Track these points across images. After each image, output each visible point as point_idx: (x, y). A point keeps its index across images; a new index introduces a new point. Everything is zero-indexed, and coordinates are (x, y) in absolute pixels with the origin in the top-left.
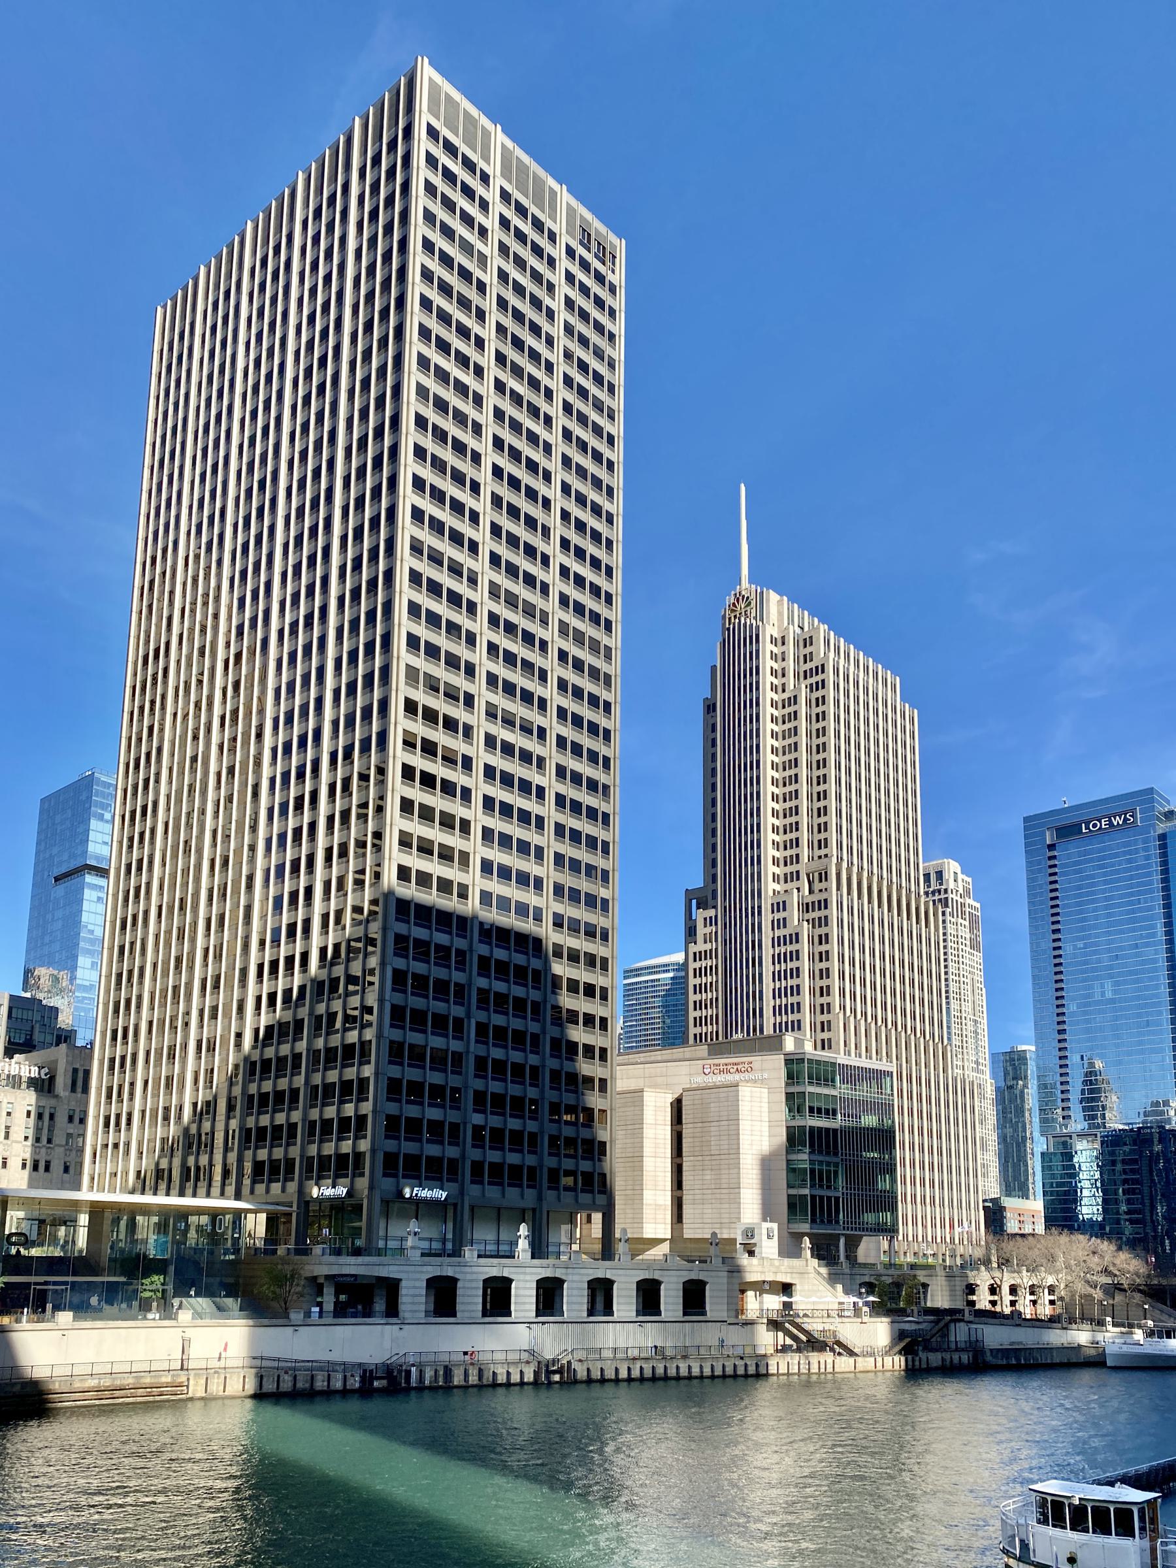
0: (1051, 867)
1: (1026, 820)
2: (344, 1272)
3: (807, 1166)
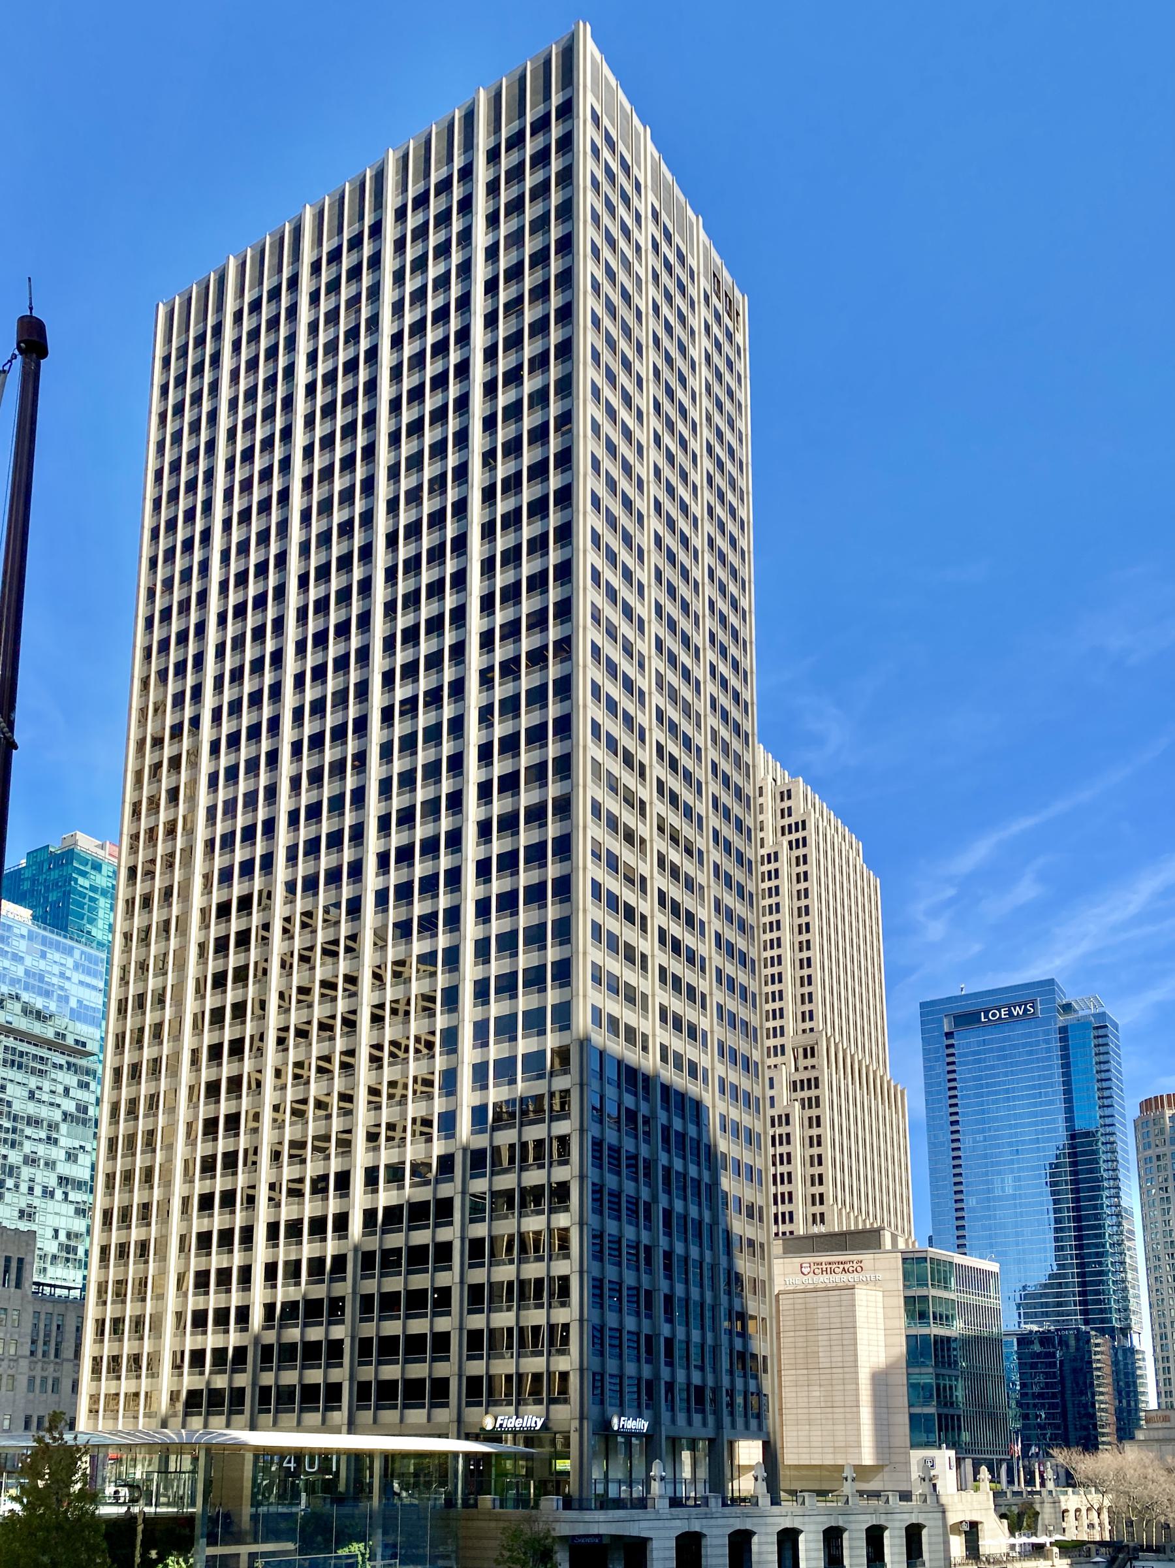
0: (948, 1055)
1: (922, 1005)
2: (591, 1532)
3: (933, 1382)
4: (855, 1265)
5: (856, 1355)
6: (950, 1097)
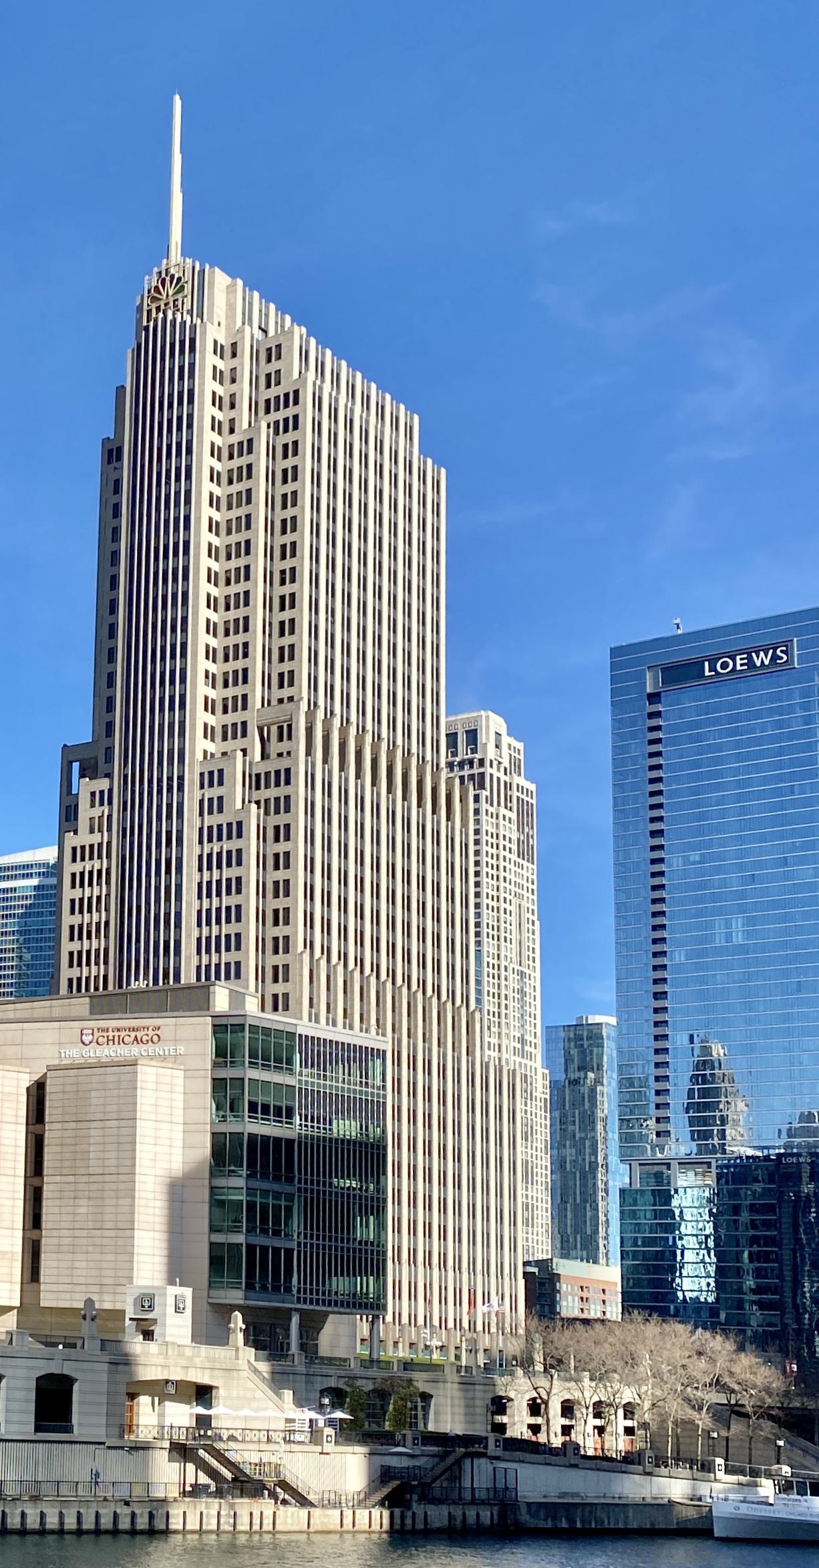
0: (652, 729)
1: (615, 652)
3: (243, 1197)
4: (151, 1033)
5: (134, 1158)
6: (652, 794)
